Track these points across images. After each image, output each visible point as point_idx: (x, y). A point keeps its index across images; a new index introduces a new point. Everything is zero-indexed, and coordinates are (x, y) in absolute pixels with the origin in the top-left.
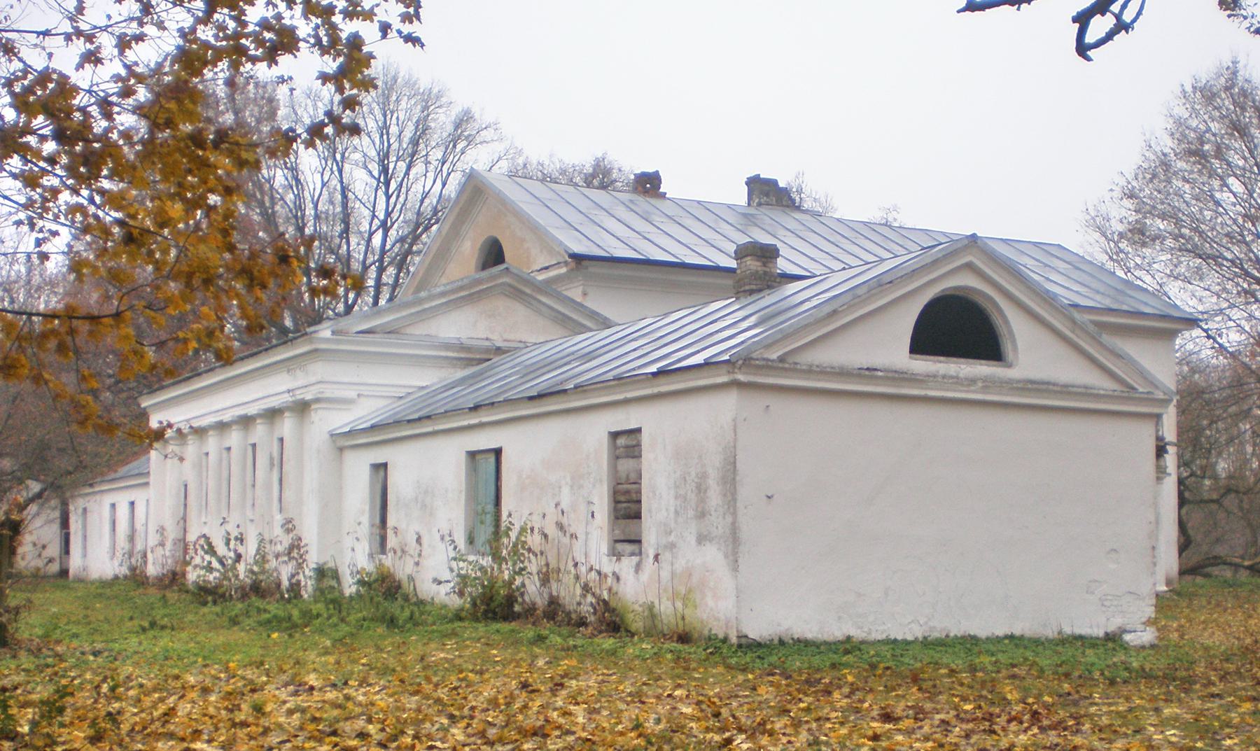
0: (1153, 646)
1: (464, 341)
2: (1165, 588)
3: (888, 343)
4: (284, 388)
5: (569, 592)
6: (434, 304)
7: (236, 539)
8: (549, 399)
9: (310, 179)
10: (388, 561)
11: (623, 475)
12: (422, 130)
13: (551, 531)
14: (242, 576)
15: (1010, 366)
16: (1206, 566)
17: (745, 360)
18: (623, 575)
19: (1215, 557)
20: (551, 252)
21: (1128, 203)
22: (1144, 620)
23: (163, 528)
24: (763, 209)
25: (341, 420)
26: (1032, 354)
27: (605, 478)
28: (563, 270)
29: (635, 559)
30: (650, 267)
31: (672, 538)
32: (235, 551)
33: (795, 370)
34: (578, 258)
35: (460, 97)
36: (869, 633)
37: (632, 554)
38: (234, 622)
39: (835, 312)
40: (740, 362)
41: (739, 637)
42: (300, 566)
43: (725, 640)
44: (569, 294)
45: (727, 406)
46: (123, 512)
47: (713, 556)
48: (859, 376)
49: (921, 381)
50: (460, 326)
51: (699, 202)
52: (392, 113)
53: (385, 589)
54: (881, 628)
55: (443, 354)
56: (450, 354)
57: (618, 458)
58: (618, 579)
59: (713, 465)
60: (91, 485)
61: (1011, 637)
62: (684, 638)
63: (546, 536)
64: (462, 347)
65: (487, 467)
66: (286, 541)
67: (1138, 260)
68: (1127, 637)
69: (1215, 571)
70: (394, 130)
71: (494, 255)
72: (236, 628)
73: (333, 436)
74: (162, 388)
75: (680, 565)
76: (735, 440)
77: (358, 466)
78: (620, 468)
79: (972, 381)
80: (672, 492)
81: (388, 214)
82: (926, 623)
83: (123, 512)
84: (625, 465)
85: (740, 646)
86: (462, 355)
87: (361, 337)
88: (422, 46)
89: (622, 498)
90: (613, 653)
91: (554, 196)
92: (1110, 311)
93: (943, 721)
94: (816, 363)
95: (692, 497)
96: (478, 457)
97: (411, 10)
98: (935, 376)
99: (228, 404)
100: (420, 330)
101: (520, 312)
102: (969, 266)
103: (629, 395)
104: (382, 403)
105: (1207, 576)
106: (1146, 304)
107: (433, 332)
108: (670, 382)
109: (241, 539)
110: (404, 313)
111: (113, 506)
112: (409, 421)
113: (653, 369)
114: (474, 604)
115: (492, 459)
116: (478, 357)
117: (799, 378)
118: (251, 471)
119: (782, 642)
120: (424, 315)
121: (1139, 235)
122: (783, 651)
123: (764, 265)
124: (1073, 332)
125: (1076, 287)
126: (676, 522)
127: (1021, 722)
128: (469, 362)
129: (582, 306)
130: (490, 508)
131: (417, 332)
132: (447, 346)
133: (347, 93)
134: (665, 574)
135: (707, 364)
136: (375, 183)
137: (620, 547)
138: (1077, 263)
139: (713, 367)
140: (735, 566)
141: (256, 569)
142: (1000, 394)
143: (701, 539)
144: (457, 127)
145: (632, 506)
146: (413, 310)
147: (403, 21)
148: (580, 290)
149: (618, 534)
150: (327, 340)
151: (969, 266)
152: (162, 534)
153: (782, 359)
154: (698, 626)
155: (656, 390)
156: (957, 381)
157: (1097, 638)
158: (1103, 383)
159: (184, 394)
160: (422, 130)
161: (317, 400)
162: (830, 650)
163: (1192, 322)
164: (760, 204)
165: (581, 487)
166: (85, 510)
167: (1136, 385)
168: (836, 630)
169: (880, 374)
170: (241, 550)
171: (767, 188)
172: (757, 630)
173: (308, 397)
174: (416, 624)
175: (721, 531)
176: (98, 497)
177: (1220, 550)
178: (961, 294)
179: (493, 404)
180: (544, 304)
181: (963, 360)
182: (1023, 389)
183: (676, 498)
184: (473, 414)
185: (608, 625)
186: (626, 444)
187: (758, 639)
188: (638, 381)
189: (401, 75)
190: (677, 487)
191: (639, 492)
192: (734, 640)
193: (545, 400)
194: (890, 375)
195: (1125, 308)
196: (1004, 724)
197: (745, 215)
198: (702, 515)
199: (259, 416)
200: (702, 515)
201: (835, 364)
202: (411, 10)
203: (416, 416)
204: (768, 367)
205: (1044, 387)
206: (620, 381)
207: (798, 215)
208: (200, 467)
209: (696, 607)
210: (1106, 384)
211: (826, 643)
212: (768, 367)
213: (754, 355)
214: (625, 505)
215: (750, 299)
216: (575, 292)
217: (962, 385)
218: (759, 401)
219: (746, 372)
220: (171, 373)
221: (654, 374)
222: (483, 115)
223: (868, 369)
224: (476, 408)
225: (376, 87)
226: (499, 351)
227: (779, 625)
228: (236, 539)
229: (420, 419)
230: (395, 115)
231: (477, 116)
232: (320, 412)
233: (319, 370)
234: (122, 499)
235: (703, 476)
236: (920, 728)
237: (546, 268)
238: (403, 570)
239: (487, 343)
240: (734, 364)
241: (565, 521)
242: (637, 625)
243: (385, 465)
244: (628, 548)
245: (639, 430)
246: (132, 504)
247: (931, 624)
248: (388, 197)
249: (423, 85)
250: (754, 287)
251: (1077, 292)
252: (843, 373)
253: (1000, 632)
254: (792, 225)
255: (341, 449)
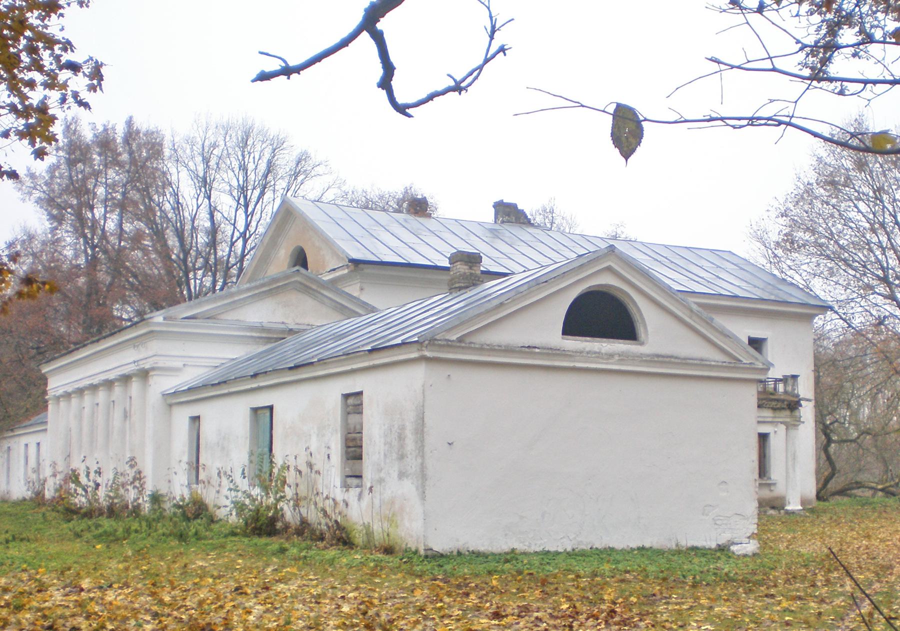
0: (754, 555)
1: (264, 324)
2: (801, 508)
3: (546, 328)
4: (131, 360)
5: (313, 516)
6: (242, 297)
7: (96, 472)
8: (301, 370)
9: (189, 203)
10: (199, 489)
11: (352, 426)
12: (270, 168)
13: (304, 468)
14: (101, 500)
15: (642, 344)
16: (853, 488)
17: (429, 341)
18: (351, 502)
19: (857, 483)
20: (338, 257)
21: (782, 221)
22: (748, 535)
23: (55, 463)
24: (506, 226)
25: (162, 384)
26: (658, 333)
27: (339, 429)
28: (346, 271)
29: (358, 490)
30: (414, 269)
31: (382, 475)
32: (95, 482)
33: (470, 348)
34: (356, 263)
35: (297, 144)
36: (529, 547)
37: (357, 486)
38: (78, 535)
39: (502, 304)
40: (427, 342)
41: (425, 550)
42: (140, 492)
43: (416, 552)
44: (347, 290)
45: (418, 375)
46: (32, 450)
47: (408, 488)
48: (520, 352)
49: (570, 356)
50: (263, 313)
51: (456, 220)
52: (250, 153)
53: (197, 510)
54: (539, 542)
55: (248, 334)
56: (254, 334)
57: (349, 413)
58: (347, 505)
59: (410, 417)
60: (12, 430)
61: (642, 549)
62: (389, 550)
63: (300, 472)
64: (263, 329)
65: (263, 417)
66: (131, 473)
67: (789, 262)
68: (734, 548)
69: (858, 492)
70: (251, 167)
71: (301, 259)
72: (78, 540)
73: (165, 395)
74: (54, 359)
75: (387, 495)
76: (424, 401)
77: (182, 417)
78: (349, 421)
79: (611, 356)
80: (382, 440)
81: (247, 226)
82: (575, 538)
83: (32, 450)
84: (353, 419)
85: (426, 557)
86: (264, 335)
87: (187, 322)
88: (90, 108)
89: (351, 444)
90: (332, 562)
91: (345, 216)
92: (762, 300)
93: (537, 618)
94: (488, 343)
95: (395, 443)
96: (259, 412)
97: (95, 82)
98: (581, 352)
99: (98, 371)
100: (232, 316)
101: (308, 303)
102: (609, 269)
103: (355, 366)
104: (206, 370)
105: (850, 496)
106: (791, 295)
107: (242, 318)
108: (380, 354)
109: (99, 473)
110: (219, 304)
111: (27, 445)
112: (213, 385)
113: (369, 348)
114: (246, 524)
115: (268, 414)
116: (275, 336)
117: (470, 354)
118: (131, 419)
119: (459, 554)
120: (234, 306)
121: (790, 243)
122: (459, 560)
123: (471, 268)
124: (691, 318)
125: (743, 285)
126: (385, 463)
127: (597, 619)
128: (269, 340)
129: (359, 299)
130: (267, 450)
131: (229, 318)
132: (252, 328)
133: (37, 146)
134: (377, 502)
135: (404, 343)
136: (235, 204)
137: (349, 480)
138: (743, 265)
139: (408, 346)
140: (423, 496)
141: (112, 494)
142: (634, 365)
143: (402, 475)
144: (298, 163)
145: (358, 450)
146: (226, 302)
147: (89, 90)
148: (358, 286)
149: (348, 471)
150: (159, 324)
151: (609, 269)
152: (54, 467)
153: (460, 340)
154: (399, 541)
155: (371, 363)
156: (599, 355)
157: (710, 549)
158: (716, 356)
159: (71, 363)
160: (270, 168)
161: (153, 369)
162: (495, 559)
163: (825, 308)
164: (503, 222)
165: (323, 436)
166: (9, 448)
167: (741, 358)
168: (502, 545)
169: (537, 350)
170: (99, 480)
171: (508, 210)
172: (439, 546)
173: (147, 366)
174: (199, 539)
175: (414, 469)
176: (16, 439)
177: (863, 477)
178: (604, 290)
179: (266, 372)
180: (327, 297)
181: (605, 340)
182: (651, 361)
183: (385, 444)
184: (254, 380)
185: (339, 540)
186: (353, 403)
187: (441, 551)
188: (361, 356)
189: (256, 126)
190: (386, 436)
191: (361, 440)
192: (422, 552)
193: (300, 370)
194: (545, 351)
195: (773, 298)
196: (583, 620)
197: (491, 230)
198: (402, 457)
199: (116, 380)
200: (402, 457)
201: (503, 343)
202: (95, 82)
203: (217, 382)
204: (448, 346)
205: (668, 360)
206: (349, 355)
207: (531, 230)
208: (80, 417)
209: (397, 527)
210: (718, 357)
211: (493, 554)
212: (449, 345)
213: (438, 337)
214: (353, 449)
215: (459, 293)
216: (353, 289)
217: (603, 358)
218: (442, 372)
219: (435, 349)
220: (59, 347)
221: (369, 351)
222: (317, 156)
223: (529, 347)
224: (255, 376)
225: (57, 141)
226: (291, 331)
227: (458, 540)
228: (96, 472)
229: (219, 383)
230: (252, 155)
231: (312, 156)
232: (155, 377)
233: (155, 347)
234: (32, 440)
235: (402, 428)
236: (518, 623)
237: (334, 270)
238: (209, 497)
239: (283, 326)
240: (422, 343)
241: (313, 461)
242: (359, 538)
243: (199, 417)
244: (355, 481)
245: (360, 394)
246: (38, 444)
247: (580, 539)
248: (247, 216)
249: (272, 133)
250: (463, 285)
251: (739, 286)
252: (508, 350)
253: (634, 545)
254: (526, 237)
255: (170, 406)
